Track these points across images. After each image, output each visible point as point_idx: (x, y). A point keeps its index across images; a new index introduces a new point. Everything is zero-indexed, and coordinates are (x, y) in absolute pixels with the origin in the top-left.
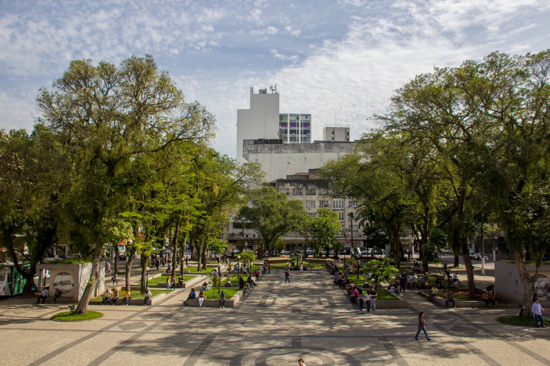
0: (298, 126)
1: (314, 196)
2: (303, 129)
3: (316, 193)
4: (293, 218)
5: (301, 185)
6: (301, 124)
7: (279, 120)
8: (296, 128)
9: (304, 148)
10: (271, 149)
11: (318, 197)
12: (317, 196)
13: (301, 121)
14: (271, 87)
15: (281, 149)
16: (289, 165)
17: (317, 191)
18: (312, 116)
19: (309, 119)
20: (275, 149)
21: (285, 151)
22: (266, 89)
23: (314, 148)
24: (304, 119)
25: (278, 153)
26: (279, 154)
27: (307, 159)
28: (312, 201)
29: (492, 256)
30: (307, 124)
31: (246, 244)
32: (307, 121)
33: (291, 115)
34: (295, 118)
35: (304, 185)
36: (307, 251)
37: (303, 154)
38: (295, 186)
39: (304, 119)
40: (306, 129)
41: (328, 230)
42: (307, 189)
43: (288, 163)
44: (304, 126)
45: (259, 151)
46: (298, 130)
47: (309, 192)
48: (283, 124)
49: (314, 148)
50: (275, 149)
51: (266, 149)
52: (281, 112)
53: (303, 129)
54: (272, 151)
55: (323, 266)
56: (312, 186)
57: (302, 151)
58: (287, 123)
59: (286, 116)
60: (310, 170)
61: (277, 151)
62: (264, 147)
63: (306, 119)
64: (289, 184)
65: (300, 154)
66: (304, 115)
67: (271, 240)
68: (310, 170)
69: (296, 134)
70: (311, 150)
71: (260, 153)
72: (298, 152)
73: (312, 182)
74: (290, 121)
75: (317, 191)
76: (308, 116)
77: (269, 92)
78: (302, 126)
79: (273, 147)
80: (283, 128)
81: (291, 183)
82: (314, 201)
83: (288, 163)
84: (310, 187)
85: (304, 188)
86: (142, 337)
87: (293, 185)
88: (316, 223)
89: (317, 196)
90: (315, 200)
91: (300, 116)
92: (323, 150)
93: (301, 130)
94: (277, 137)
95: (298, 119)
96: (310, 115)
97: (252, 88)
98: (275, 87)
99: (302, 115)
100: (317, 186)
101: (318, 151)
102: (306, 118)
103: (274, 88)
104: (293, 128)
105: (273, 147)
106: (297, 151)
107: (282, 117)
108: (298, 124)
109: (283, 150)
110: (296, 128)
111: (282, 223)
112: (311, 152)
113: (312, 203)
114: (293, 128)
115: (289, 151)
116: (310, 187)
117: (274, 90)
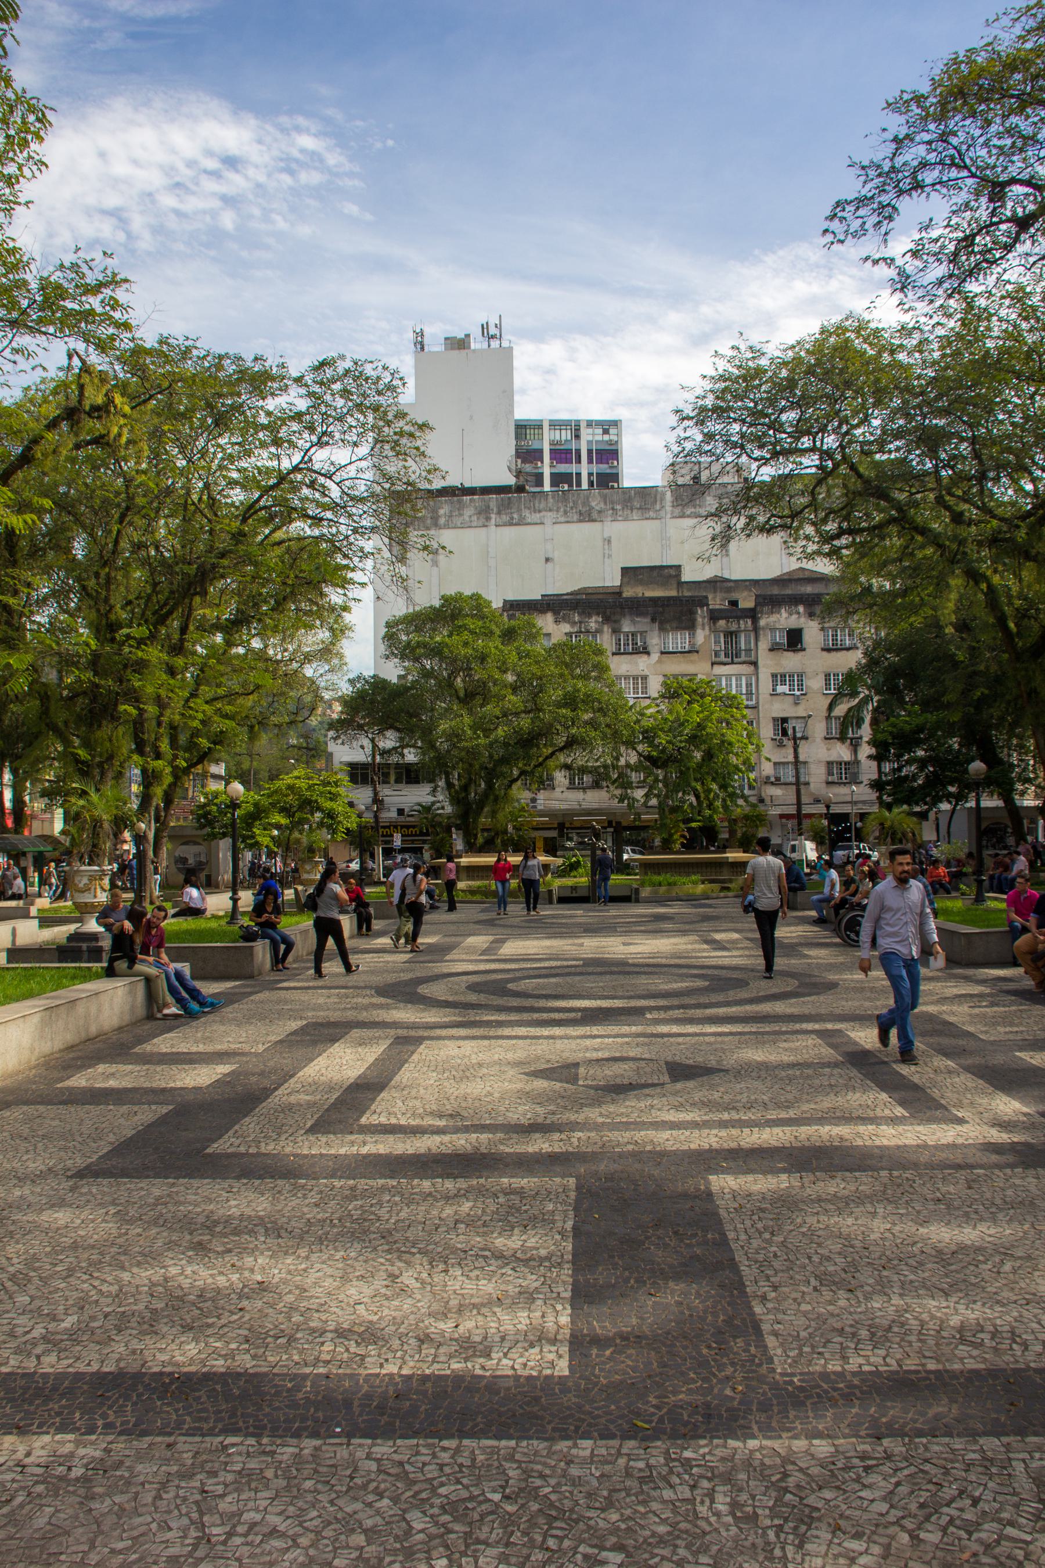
0: (579, 461)
1: (645, 657)
2: (595, 468)
3: (650, 649)
4: (571, 701)
5: (594, 619)
6: (590, 452)
7: (514, 442)
8: (573, 468)
9: (602, 505)
10: (484, 513)
11: (659, 661)
12: (655, 656)
13: (589, 442)
14: (484, 328)
15: (519, 510)
16: (550, 565)
17: (654, 641)
18: (624, 424)
19: (615, 438)
20: (499, 513)
21: (536, 517)
22: (468, 336)
23: (637, 504)
24: (599, 438)
25: (511, 524)
26: (513, 529)
27: (614, 543)
28: (635, 678)
29: (81, 961)
30: (609, 454)
31: (397, 841)
32: (610, 443)
33: (555, 425)
34: (566, 435)
35: (607, 620)
36: (625, 857)
37: (597, 526)
38: (573, 624)
39: (598, 435)
40: (604, 468)
41: (709, 756)
42: (616, 631)
43: (547, 560)
44: (600, 461)
45: (442, 521)
46: (579, 475)
47: (626, 644)
48: (527, 455)
49: (637, 504)
50: (499, 513)
51: (468, 512)
52: (524, 411)
53: (595, 468)
54: (488, 519)
55: (712, 881)
56: (634, 622)
57: (595, 515)
58: (541, 451)
59: (538, 426)
60: (625, 571)
61: (505, 518)
62: (461, 507)
63: (606, 438)
64: (549, 617)
65: (587, 527)
66: (599, 423)
67: (481, 804)
68: (625, 571)
69: (571, 485)
70: (627, 512)
71: (446, 526)
72: (580, 521)
73: (637, 607)
74: (552, 443)
75: (654, 641)
76: (608, 426)
77: (477, 344)
78: (590, 461)
79: (493, 505)
80: (528, 468)
81: (556, 613)
82: (645, 678)
83: (547, 560)
84: (627, 627)
85: (606, 629)
86: (371, 1059)
87: (566, 619)
88: (662, 730)
89: (655, 656)
90: (646, 672)
91: (583, 425)
92: (668, 508)
93: (590, 475)
94: (511, 480)
95: (578, 437)
96: (615, 423)
97: (422, 334)
98: (498, 326)
99: (590, 424)
100: (653, 620)
101: (651, 514)
102: (606, 432)
103: (493, 331)
104: (563, 468)
105: (493, 505)
106: (576, 517)
107: (522, 429)
108: (578, 452)
109: (526, 513)
110: (573, 468)
111: (525, 722)
112: (626, 520)
113: (636, 684)
114: (563, 468)
115: (549, 517)
116: (627, 627)
117: (493, 337)
